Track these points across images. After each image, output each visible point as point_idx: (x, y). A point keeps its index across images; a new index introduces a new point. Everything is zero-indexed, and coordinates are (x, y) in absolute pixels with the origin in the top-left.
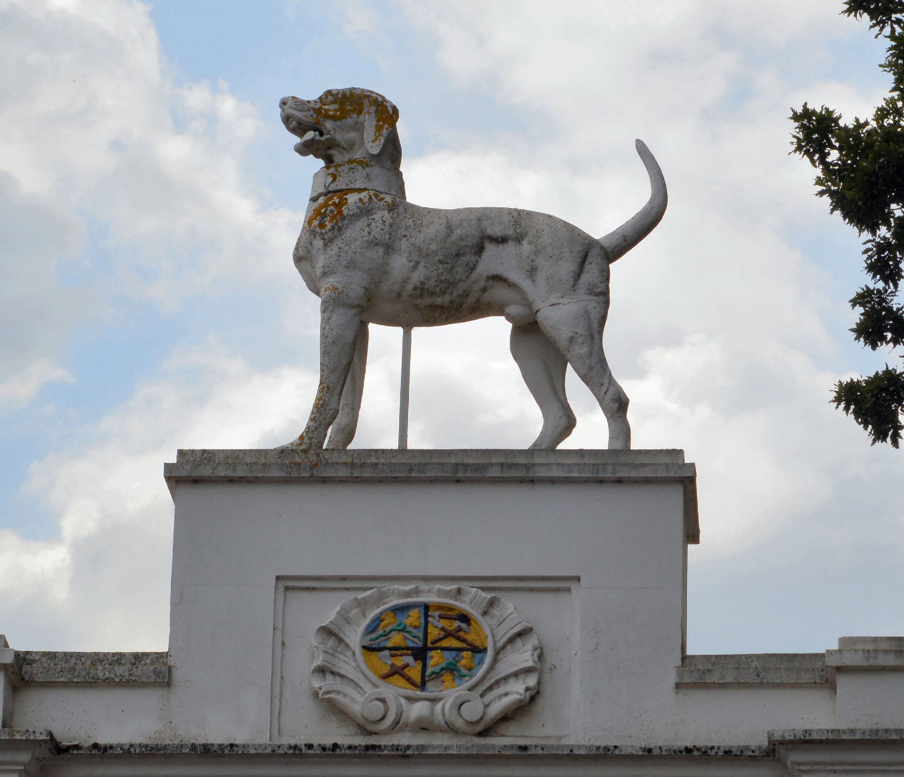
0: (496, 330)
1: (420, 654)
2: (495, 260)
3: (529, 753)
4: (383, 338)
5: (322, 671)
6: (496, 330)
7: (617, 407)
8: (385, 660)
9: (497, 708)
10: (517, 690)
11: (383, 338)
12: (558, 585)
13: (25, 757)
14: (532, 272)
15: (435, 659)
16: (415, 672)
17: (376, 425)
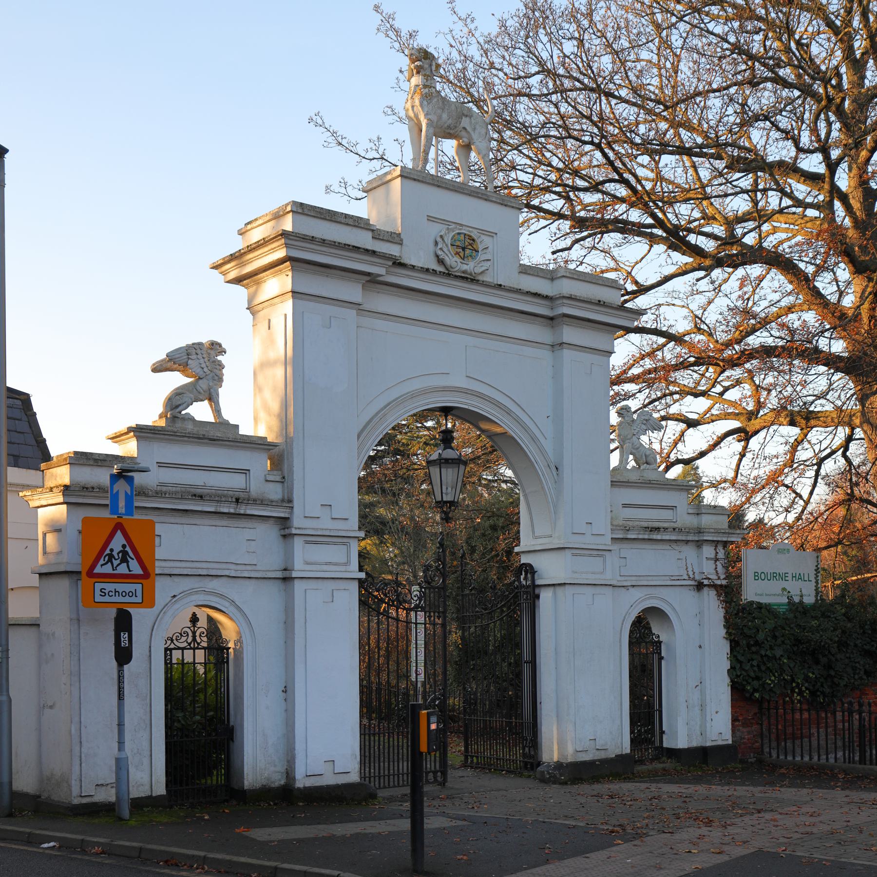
1: (464, 249)
14: (474, 129)
15: (468, 252)
16: (462, 255)
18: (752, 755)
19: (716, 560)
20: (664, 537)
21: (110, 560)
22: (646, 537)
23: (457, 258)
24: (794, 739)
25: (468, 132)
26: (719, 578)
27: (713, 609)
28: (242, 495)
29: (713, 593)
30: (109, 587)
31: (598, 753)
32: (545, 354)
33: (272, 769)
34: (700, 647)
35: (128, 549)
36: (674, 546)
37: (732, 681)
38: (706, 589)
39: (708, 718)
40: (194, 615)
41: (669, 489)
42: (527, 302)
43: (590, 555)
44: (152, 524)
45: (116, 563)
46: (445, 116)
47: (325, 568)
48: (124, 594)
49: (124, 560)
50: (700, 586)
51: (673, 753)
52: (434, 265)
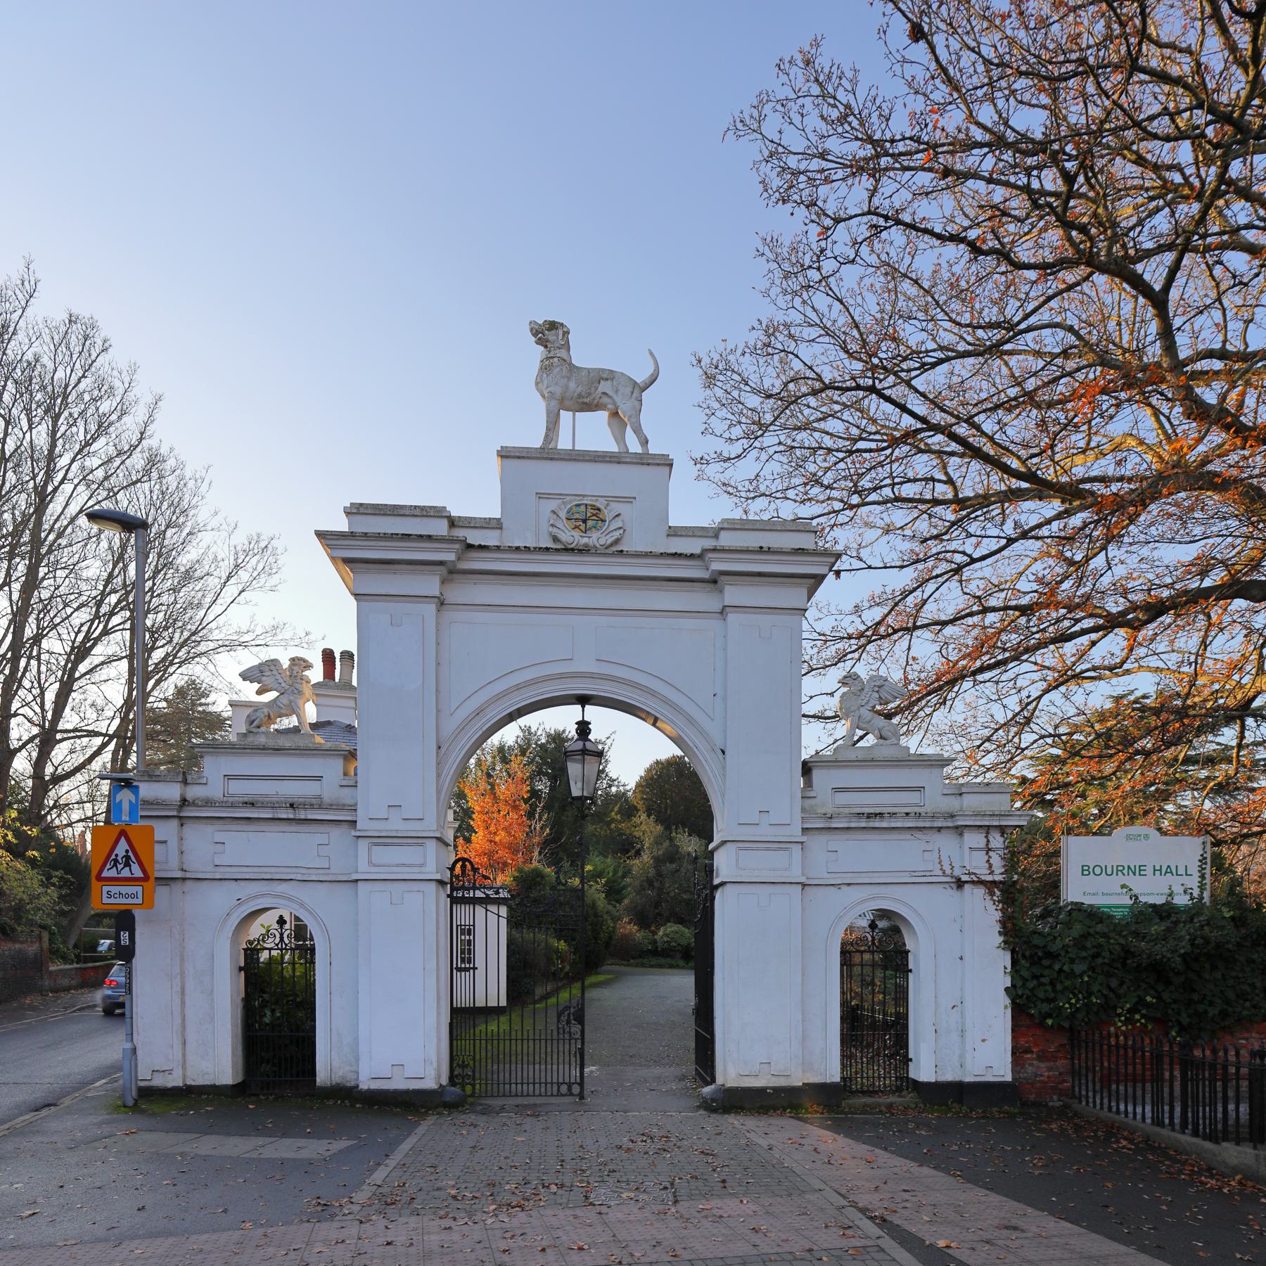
0: (603, 415)
1: (585, 521)
2: (605, 387)
3: (355, 653)
4: (565, 416)
5: (552, 525)
6: (603, 415)
7: (645, 442)
8: (573, 523)
9: (609, 541)
10: (617, 534)
11: (565, 416)
12: (629, 500)
13: (457, 546)
14: (617, 391)
15: (590, 523)
16: (583, 527)
17: (564, 443)
18: (1055, 1097)
19: (988, 850)
20: (893, 825)
21: (115, 865)
22: (863, 825)
23: (576, 534)
24: (1135, 1081)
25: (610, 397)
26: (992, 873)
27: (984, 914)
28: (314, 801)
29: (980, 891)
30: (115, 889)
31: (774, 1079)
32: (715, 624)
33: (348, 1068)
34: (961, 958)
35: (130, 854)
36: (919, 835)
37: (1013, 1003)
38: (966, 886)
39: (969, 1047)
40: (281, 917)
41: (911, 767)
42: (669, 566)
43: (768, 849)
44: (152, 829)
45: (120, 867)
46: (572, 385)
47: (395, 869)
48: (128, 896)
49: (127, 864)
50: (960, 884)
51: (917, 1086)
52: (551, 545)
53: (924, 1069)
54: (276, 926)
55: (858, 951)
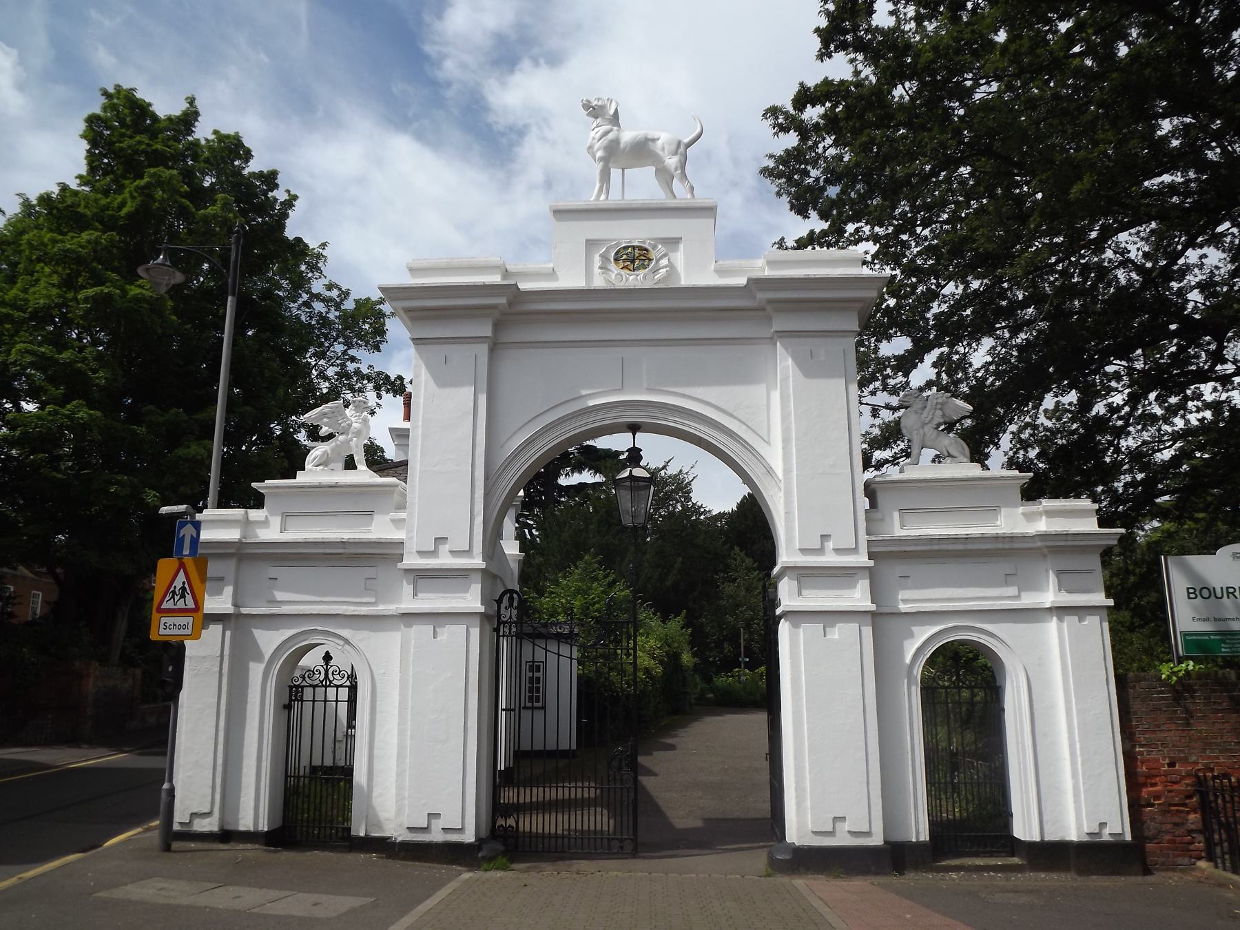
11: (615, 173)
30: (170, 621)
40: (327, 653)
53: (1024, 828)
54: (322, 663)
55: (311, 686)
